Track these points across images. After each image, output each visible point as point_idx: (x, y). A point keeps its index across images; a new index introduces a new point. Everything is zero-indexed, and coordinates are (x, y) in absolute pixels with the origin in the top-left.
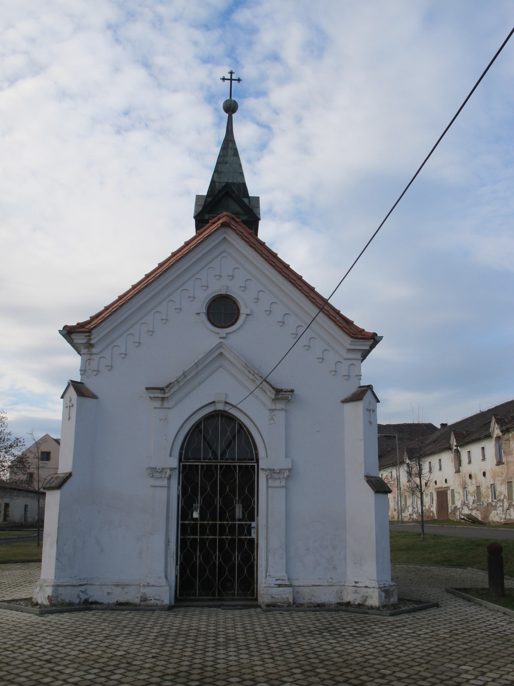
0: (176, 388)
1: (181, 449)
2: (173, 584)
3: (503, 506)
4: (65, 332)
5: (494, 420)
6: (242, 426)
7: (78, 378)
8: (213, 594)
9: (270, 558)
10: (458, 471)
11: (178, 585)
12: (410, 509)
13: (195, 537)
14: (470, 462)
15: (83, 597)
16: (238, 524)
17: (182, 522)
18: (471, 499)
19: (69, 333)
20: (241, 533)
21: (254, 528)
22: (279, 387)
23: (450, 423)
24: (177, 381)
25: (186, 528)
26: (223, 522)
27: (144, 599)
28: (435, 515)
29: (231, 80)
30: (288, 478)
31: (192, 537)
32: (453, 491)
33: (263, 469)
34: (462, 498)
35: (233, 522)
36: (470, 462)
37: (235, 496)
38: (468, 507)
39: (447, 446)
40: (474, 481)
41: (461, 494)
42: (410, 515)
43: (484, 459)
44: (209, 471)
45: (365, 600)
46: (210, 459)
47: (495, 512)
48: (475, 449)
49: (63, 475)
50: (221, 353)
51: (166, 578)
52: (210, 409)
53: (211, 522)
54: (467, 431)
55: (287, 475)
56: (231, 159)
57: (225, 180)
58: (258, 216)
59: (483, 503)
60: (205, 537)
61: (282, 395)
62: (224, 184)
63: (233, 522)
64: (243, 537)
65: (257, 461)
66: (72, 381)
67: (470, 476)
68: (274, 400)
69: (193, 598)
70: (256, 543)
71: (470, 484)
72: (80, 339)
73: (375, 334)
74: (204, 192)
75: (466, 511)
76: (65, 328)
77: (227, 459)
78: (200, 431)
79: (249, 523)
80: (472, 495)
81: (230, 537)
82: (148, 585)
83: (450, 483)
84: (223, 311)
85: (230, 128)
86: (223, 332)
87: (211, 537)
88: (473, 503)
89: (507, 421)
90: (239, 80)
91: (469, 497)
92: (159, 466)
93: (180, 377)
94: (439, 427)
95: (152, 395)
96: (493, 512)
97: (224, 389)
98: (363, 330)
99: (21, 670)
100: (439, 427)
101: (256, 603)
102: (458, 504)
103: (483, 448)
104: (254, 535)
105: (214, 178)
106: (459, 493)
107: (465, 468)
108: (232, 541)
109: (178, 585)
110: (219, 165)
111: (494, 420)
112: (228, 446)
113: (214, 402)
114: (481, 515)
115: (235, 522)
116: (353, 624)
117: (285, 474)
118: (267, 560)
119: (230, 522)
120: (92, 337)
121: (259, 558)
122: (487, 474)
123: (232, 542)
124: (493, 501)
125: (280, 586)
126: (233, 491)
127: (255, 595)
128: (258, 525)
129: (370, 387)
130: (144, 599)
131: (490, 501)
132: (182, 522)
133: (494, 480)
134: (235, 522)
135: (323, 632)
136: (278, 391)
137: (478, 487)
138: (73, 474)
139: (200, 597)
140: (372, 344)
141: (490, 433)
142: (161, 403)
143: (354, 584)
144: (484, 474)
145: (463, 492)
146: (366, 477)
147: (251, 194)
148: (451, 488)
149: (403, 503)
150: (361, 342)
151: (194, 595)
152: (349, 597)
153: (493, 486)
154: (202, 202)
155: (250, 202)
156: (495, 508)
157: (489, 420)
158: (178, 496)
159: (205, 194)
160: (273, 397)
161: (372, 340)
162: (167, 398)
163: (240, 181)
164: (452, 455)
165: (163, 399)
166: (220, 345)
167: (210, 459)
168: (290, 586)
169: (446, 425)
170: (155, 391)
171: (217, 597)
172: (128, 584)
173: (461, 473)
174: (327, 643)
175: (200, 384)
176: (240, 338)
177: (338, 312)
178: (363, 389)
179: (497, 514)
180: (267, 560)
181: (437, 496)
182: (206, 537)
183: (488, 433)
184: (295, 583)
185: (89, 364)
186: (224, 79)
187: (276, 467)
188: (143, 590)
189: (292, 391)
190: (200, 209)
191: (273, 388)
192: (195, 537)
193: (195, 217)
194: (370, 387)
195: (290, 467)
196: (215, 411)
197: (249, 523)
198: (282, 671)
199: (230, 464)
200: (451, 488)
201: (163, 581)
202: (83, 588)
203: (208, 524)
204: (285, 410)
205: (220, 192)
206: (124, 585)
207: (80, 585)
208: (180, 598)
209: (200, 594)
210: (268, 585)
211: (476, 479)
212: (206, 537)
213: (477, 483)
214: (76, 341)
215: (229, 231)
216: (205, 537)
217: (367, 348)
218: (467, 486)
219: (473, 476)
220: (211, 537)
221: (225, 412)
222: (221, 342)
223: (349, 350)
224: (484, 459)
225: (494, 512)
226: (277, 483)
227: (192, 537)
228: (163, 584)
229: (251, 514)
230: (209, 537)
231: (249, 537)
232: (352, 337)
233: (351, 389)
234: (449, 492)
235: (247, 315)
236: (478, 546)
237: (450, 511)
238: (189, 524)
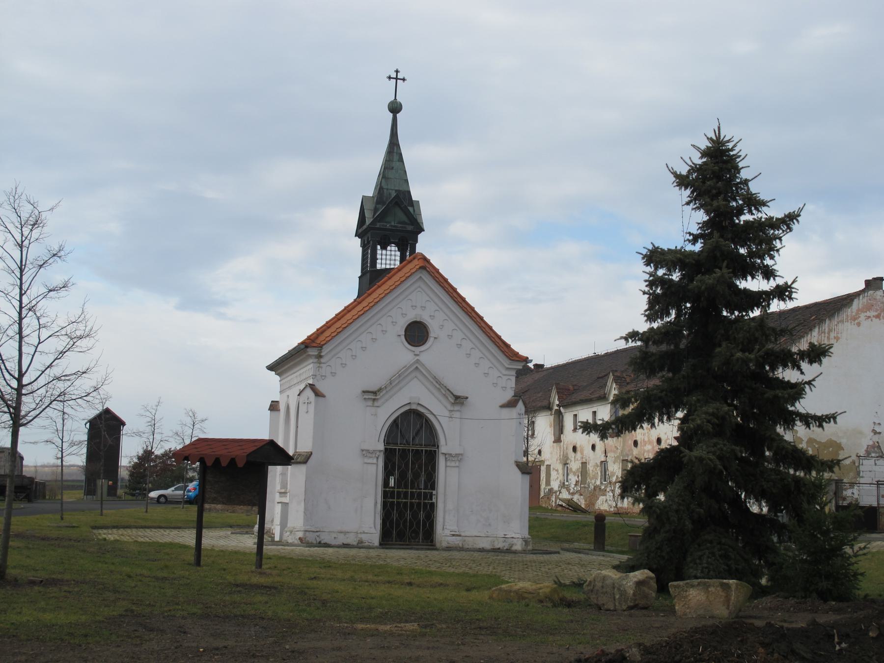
0: (384, 392)
3: (613, 491)
5: (611, 377)
6: (428, 421)
10: (558, 440)
15: (318, 540)
18: (573, 479)
20: (425, 498)
23: (548, 365)
24: (386, 387)
25: (387, 494)
27: (360, 542)
29: (397, 79)
32: (548, 466)
34: (561, 477)
38: (568, 490)
39: (545, 403)
40: (579, 454)
41: (561, 471)
44: (404, 453)
52: (407, 408)
54: (573, 386)
55: (458, 457)
56: (396, 164)
61: (459, 400)
67: (575, 449)
68: (453, 404)
75: (565, 495)
80: (574, 474)
82: (364, 533)
84: (417, 333)
86: (417, 350)
88: (576, 485)
89: (628, 380)
90: (404, 80)
91: (571, 476)
92: (371, 448)
97: (416, 394)
102: (555, 485)
104: (434, 500)
106: (557, 471)
108: (419, 504)
111: (611, 377)
112: (417, 434)
118: (444, 518)
122: (597, 448)
124: (601, 483)
125: (453, 535)
126: (420, 468)
130: (360, 542)
131: (598, 483)
136: (457, 398)
137: (584, 464)
141: (605, 394)
145: (563, 469)
146: (516, 462)
148: (546, 463)
152: (499, 545)
153: (604, 464)
156: (604, 493)
160: (453, 401)
164: (552, 418)
165: (374, 400)
168: (460, 536)
169: (542, 366)
176: (430, 355)
177: (499, 337)
180: (444, 518)
183: (602, 392)
184: (463, 534)
187: (453, 452)
188: (360, 536)
189: (467, 398)
200: (546, 463)
211: (582, 453)
215: (424, 272)
218: (568, 461)
219: (578, 449)
225: (602, 498)
226: (453, 464)
229: (431, 483)
234: (543, 468)
236: (584, 526)
237: (542, 494)
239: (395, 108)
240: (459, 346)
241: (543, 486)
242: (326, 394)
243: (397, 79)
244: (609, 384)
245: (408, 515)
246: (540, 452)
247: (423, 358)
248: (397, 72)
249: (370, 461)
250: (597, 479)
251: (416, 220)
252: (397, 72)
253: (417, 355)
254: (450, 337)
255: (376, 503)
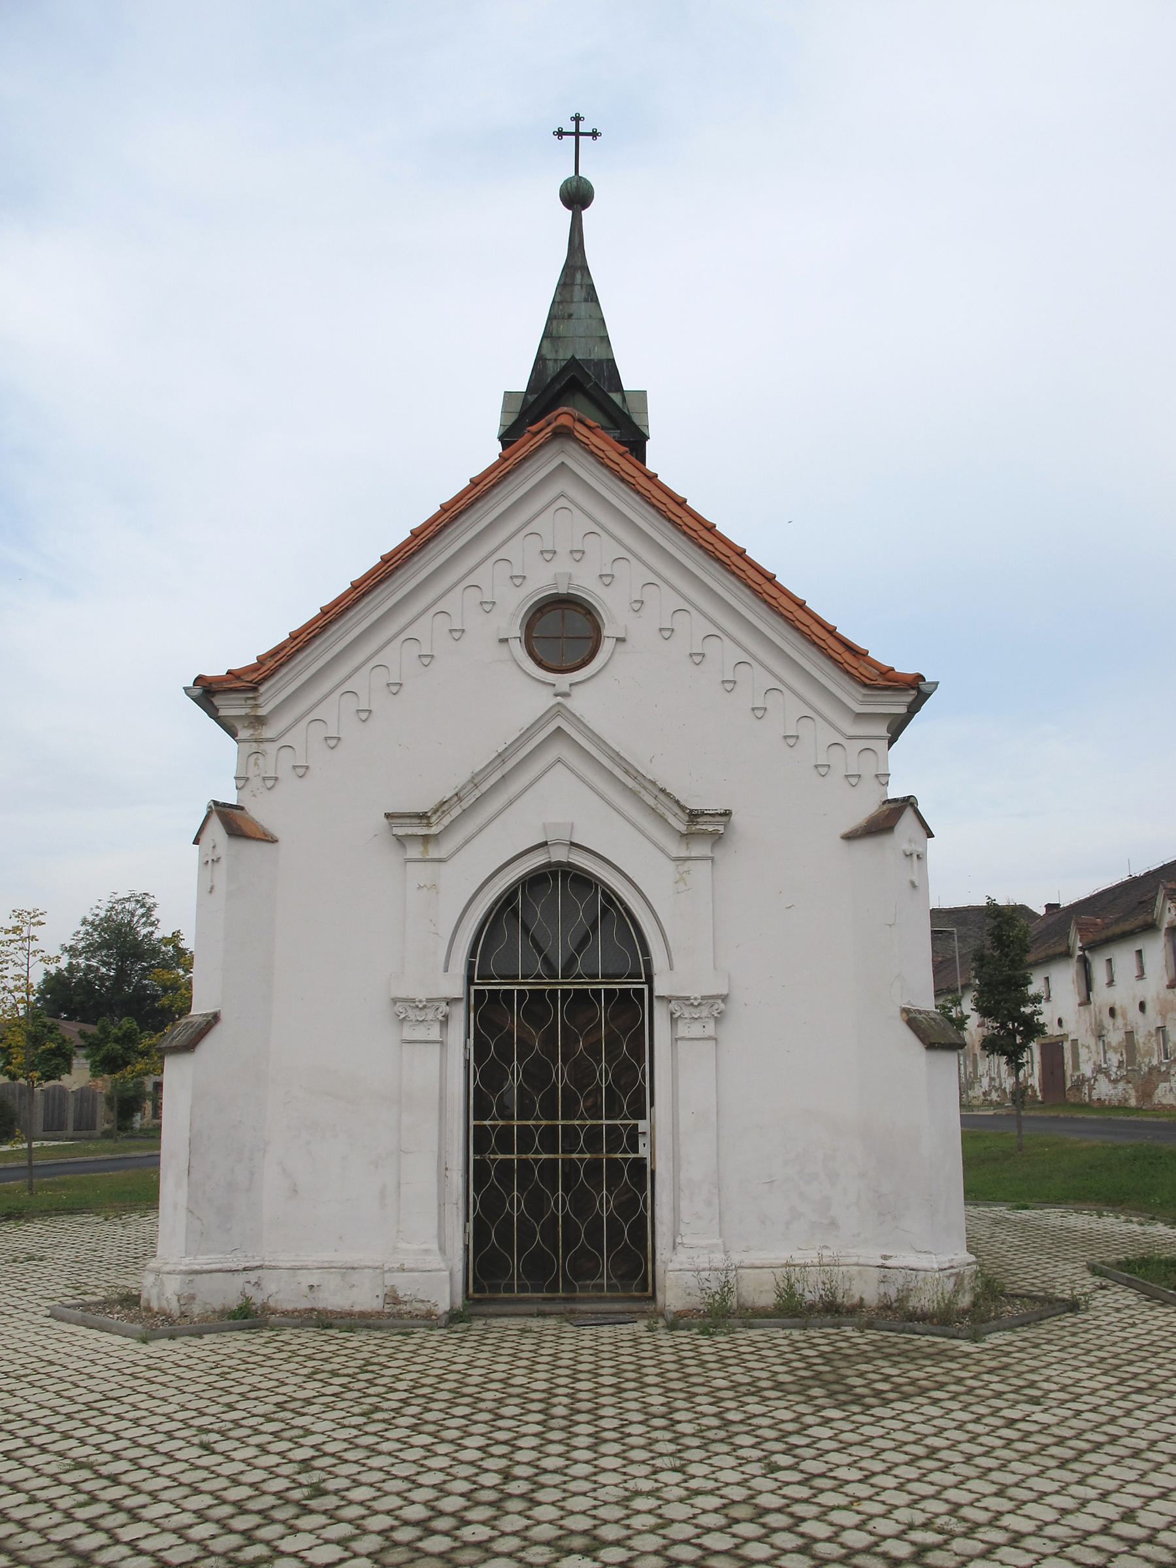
1: (473, 953)
2: (459, 1266)
4: (198, 691)
6: (611, 900)
7: (230, 797)
8: (553, 1288)
9: (684, 1204)
10: (1086, 1001)
11: (471, 1266)
12: (985, 1081)
13: (508, 1156)
14: (1111, 983)
16: (607, 1125)
17: (478, 1122)
18: (1114, 1058)
19: (207, 692)
21: (644, 1133)
22: (694, 805)
23: (1065, 903)
26: (571, 1122)
28: (1038, 1094)
29: (577, 134)
30: (719, 1019)
31: (500, 1156)
32: (1075, 1041)
33: (661, 998)
35: (594, 1122)
36: (1111, 983)
37: (599, 1062)
38: (1108, 1075)
39: (1062, 949)
40: (1119, 1021)
41: (1093, 1048)
42: (985, 1094)
43: (1141, 976)
44: (537, 1005)
45: (907, 1297)
46: (538, 976)
47: (1167, 1084)
48: (1123, 957)
49: (200, 1019)
50: (559, 729)
51: (442, 1250)
52: (536, 861)
53: (544, 1122)
55: (716, 1006)
56: (581, 309)
57: (565, 354)
58: (644, 430)
59: (1140, 1067)
60: (531, 1156)
61: (703, 828)
62: (563, 363)
63: (594, 1122)
64: (618, 1156)
65: (650, 980)
66: (216, 803)
67: (1112, 1012)
68: (686, 837)
69: (507, 1295)
70: (649, 1170)
71: (1111, 1028)
72: (231, 707)
73: (920, 678)
74: (521, 384)
76: (199, 682)
77: (579, 976)
78: (515, 911)
79: (633, 1122)
80: (1115, 1050)
81: (588, 1156)
83: (1070, 1027)
84: (562, 631)
85: (577, 242)
86: (563, 681)
87: (544, 1156)
88: (1119, 1067)
90: (594, 134)
92: (421, 994)
93: (464, 787)
94: (1041, 911)
95: (401, 831)
96: (1162, 1085)
98: (893, 669)
99: (161, 1437)
100: (1041, 911)
101: (652, 1307)
102: (1087, 1070)
103: (1139, 952)
104: (644, 1152)
105: (544, 352)
106: (1088, 1047)
107: (1102, 995)
109: (471, 1266)
110: (555, 323)
112: (580, 948)
113: (545, 844)
114: (1137, 1091)
115: (600, 1122)
116: (880, 1363)
117: (716, 1007)
118: (676, 1209)
119: (589, 1122)
120: (261, 700)
121: (657, 1202)
122: (1148, 1007)
123: (593, 1168)
127: (650, 1289)
128: (652, 1128)
129: (912, 800)
132: (478, 1122)
133: (1164, 1017)
134: (600, 1122)
135: (810, 1387)
136: (694, 816)
137: (1130, 1034)
138: (223, 1016)
139: (523, 1295)
140: (914, 701)
142: (422, 849)
143: (880, 1262)
144: (1142, 1006)
146: (905, 1011)
147: (626, 387)
148: (1071, 1037)
149: (970, 1069)
150: (888, 696)
151: (509, 1288)
154: (517, 406)
155: (624, 400)
157: (1151, 895)
158: (467, 1062)
159: (523, 388)
160: (683, 828)
161: (914, 692)
162: (436, 837)
163: (597, 353)
166: (558, 710)
167: (538, 976)
170: (408, 821)
171: (561, 1294)
172: (355, 1265)
173: (1092, 1006)
174: (818, 1420)
175: (511, 803)
176: (599, 697)
178: (892, 806)
179: (1171, 1090)
180: (676, 1209)
181: (1042, 1054)
182: (533, 1156)
185: (256, 764)
186: (560, 134)
187: (695, 993)
189: (727, 814)
190: (512, 418)
191: (683, 808)
192: (508, 1156)
193: (501, 438)
194: (912, 800)
195: (725, 992)
196: (549, 864)
197: (633, 1122)
198: (704, 1512)
199: (585, 987)
200: (1071, 1037)
201: (435, 1261)
202: (252, 1276)
203: (537, 1127)
204: (712, 859)
205: (556, 379)
206: (347, 1268)
207: (245, 1269)
208: (477, 1296)
209: (523, 1288)
210: (679, 1267)
211: (1124, 1018)
212: (533, 1156)
213: (1126, 1025)
214: (223, 712)
215: (572, 447)
216: (531, 1156)
217: (903, 710)
218: (1104, 1032)
219: (1118, 1012)
220: (544, 1156)
221: (569, 864)
222: (559, 704)
223: (860, 717)
224: (1141, 976)
226: (696, 1030)
227: (500, 1156)
228: (435, 1266)
230: (540, 1156)
231: (632, 1156)
232: (865, 685)
233: (865, 808)
234: (1067, 1046)
235: (618, 639)
237: (1069, 1084)
238: (493, 1127)
239: (577, 196)
240: (698, 658)
241: (1069, 1069)
242: (277, 833)
243: (577, 134)
244: (1159, 903)
245: (559, 1202)
246: (1060, 1022)
247: (579, 703)
248: (577, 119)
249: (419, 1033)
250: (1152, 1055)
251: (628, 419)
252: (577, 119)
253: (566, 695)
254: (667, 633)
255: (443, 1170)
